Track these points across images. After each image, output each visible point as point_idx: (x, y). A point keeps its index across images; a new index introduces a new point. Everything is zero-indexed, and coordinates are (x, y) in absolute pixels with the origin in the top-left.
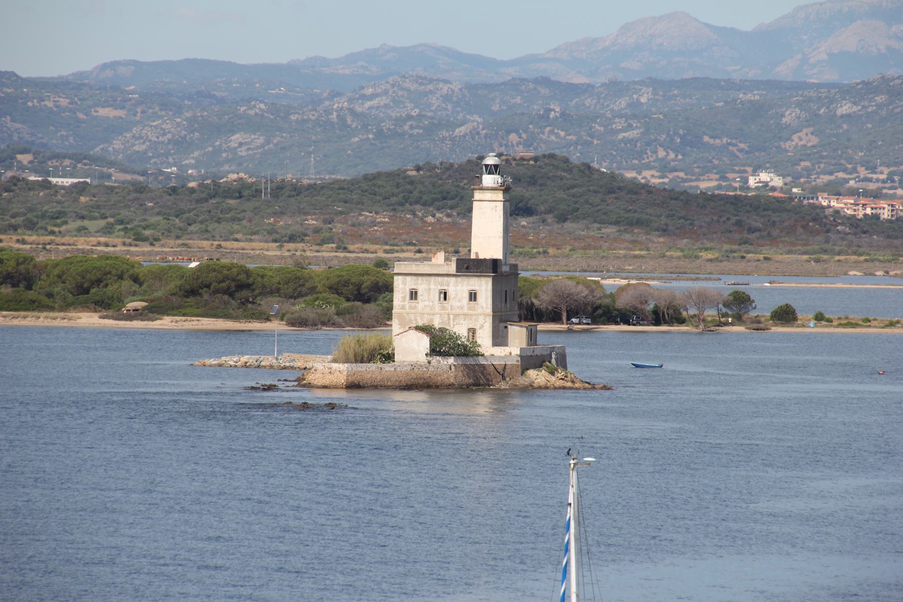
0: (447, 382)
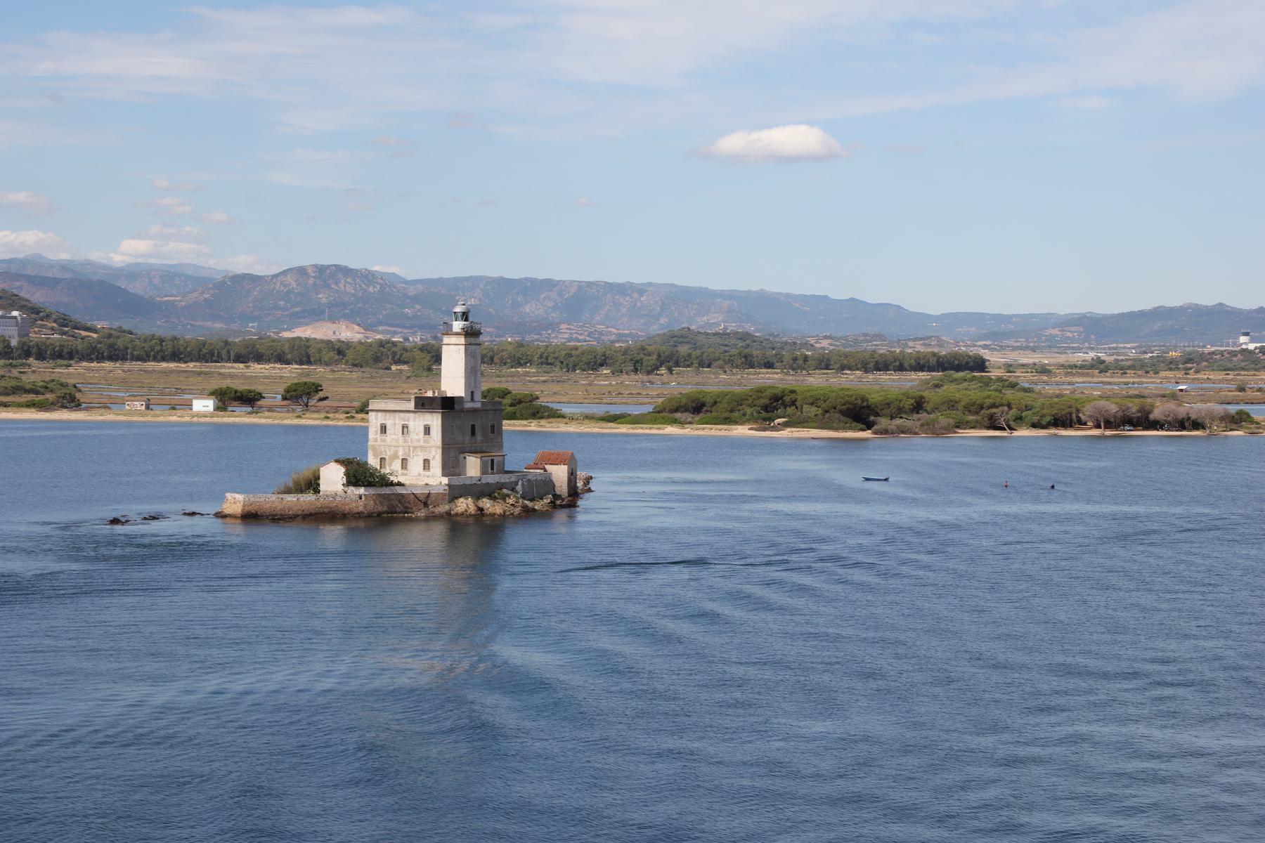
0: (356, 510)
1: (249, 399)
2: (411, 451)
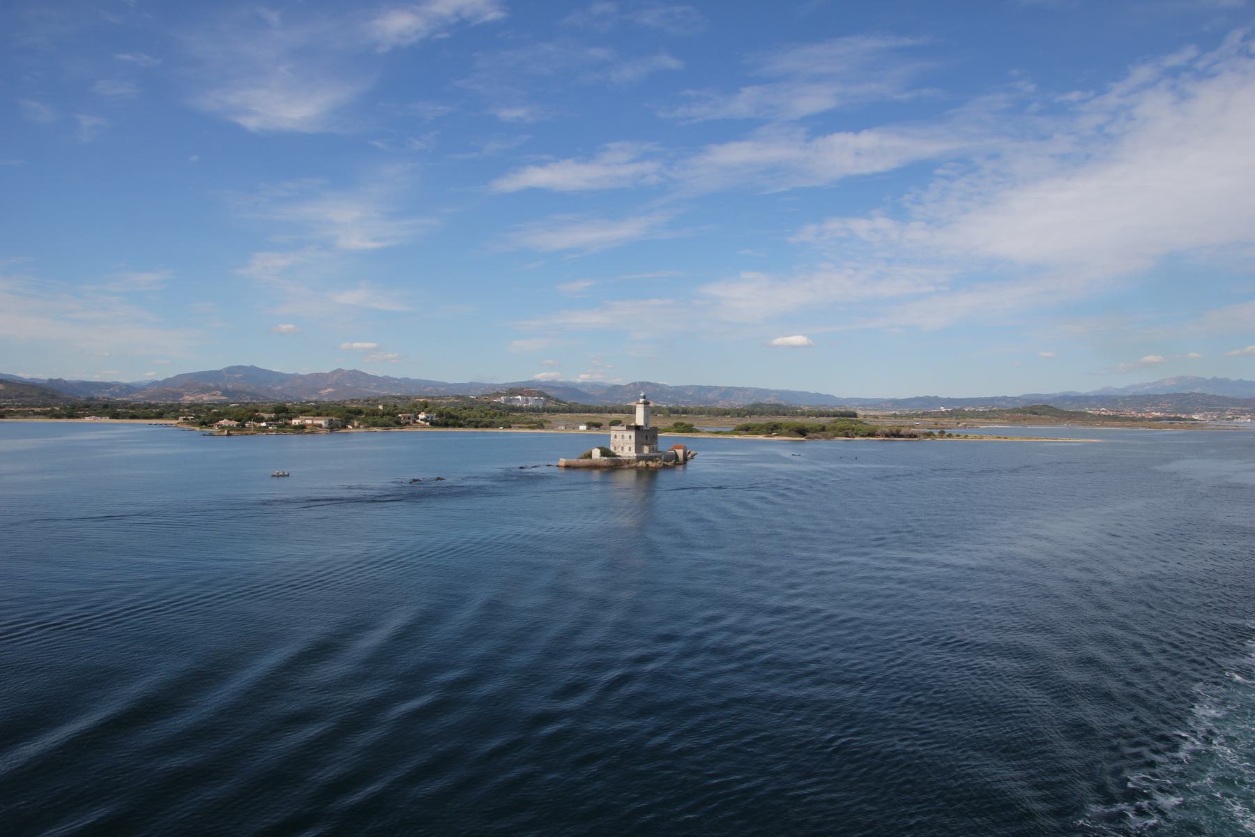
1: (598, 426)
2: (624, 444)
